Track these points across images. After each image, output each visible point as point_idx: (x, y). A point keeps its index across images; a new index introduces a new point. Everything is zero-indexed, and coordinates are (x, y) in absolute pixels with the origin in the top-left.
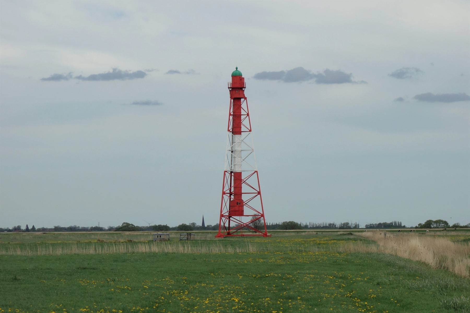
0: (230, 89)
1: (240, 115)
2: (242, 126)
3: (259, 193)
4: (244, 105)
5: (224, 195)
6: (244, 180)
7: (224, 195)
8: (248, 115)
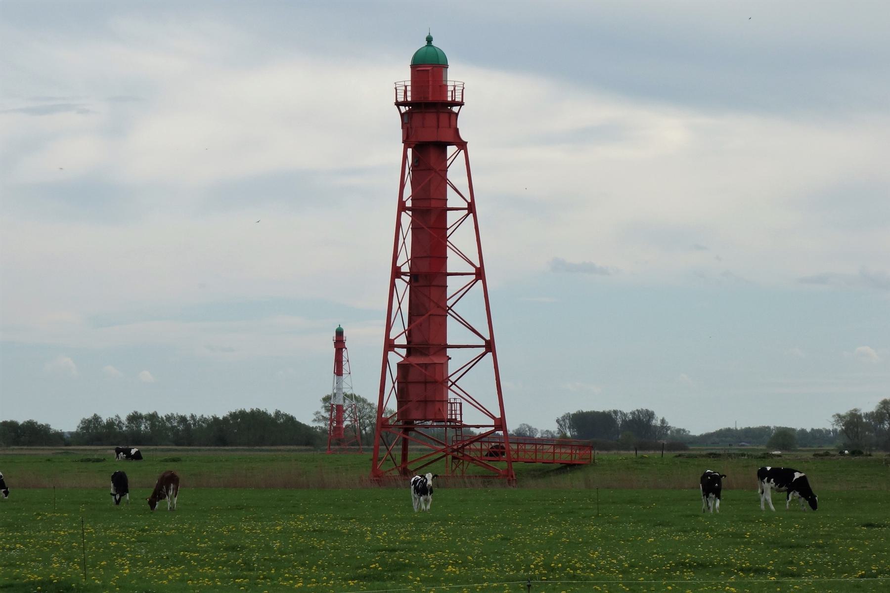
0: (403, 109)
1: (444, 210)
2: (449, 252)
3: (490, 346)
4: (455, 173)
5: (397, 281)
6: (453, 379)
7: (397, 281)
8: (480, 274)
